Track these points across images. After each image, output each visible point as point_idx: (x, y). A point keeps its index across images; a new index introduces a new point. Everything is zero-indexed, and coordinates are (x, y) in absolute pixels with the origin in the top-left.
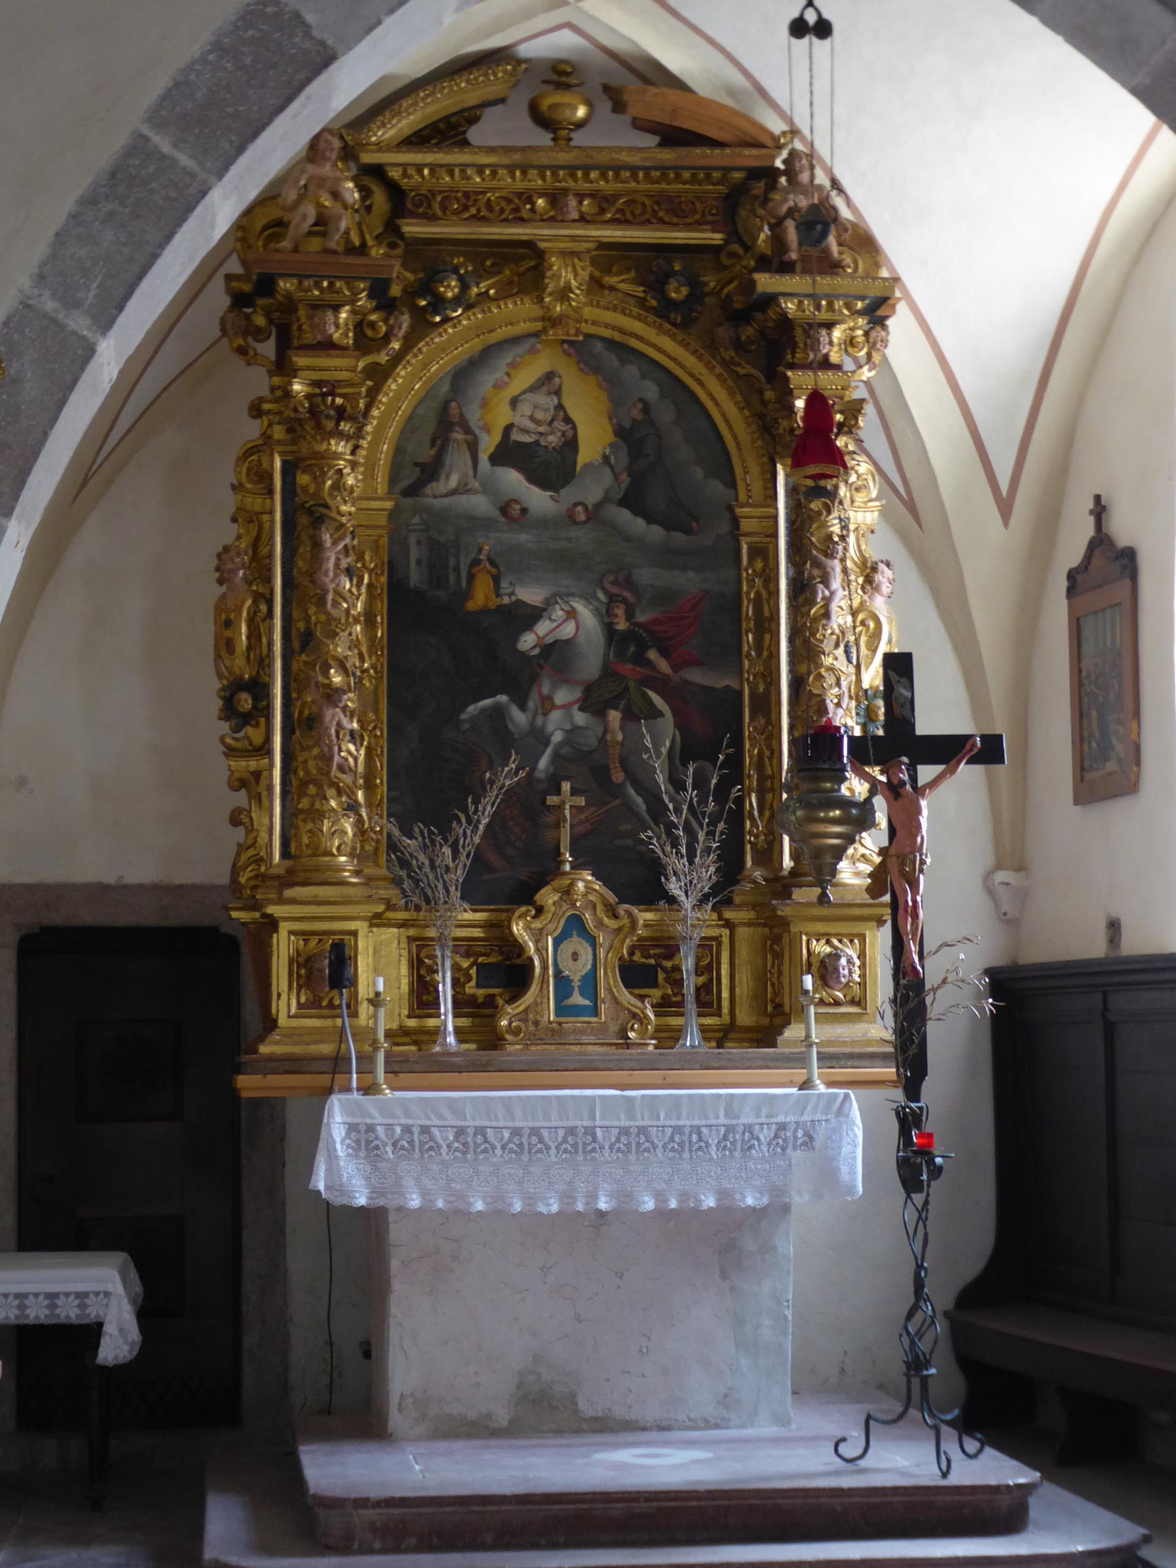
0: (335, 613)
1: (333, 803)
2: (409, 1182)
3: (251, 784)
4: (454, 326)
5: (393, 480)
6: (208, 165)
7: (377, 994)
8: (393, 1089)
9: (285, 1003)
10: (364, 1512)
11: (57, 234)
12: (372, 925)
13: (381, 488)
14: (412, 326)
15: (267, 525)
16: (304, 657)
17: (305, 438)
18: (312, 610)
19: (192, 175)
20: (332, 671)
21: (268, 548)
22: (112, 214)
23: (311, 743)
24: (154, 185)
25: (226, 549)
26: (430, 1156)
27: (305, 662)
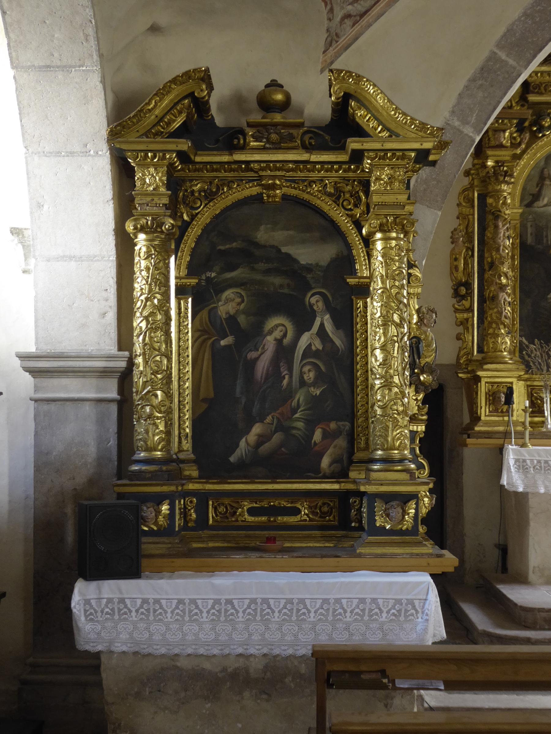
0: (503, 254)
1: (503, 331)
2: (540, 483)
3: (465, 324)
4: (547, 138)
5: (522, 200)
6: (521, 63)
7: (526, 407)
8: (533, 445)
9: (484, 411)
10: (542, 614)
11: (459, 94)
12: (518, 380)
13: (517, 203)
14: (530, 139)
15: (471, 220)
16: (490, 272)
17: (491, 184)
18: (494, 253)
19: (514, 68)
20: (502, 278)
21: (471, 229)
22: (481, 85)
23: (494, 307)
24: (499, 73)
25: (455, 230)
26: (548, 473)
27: (491, 274)
